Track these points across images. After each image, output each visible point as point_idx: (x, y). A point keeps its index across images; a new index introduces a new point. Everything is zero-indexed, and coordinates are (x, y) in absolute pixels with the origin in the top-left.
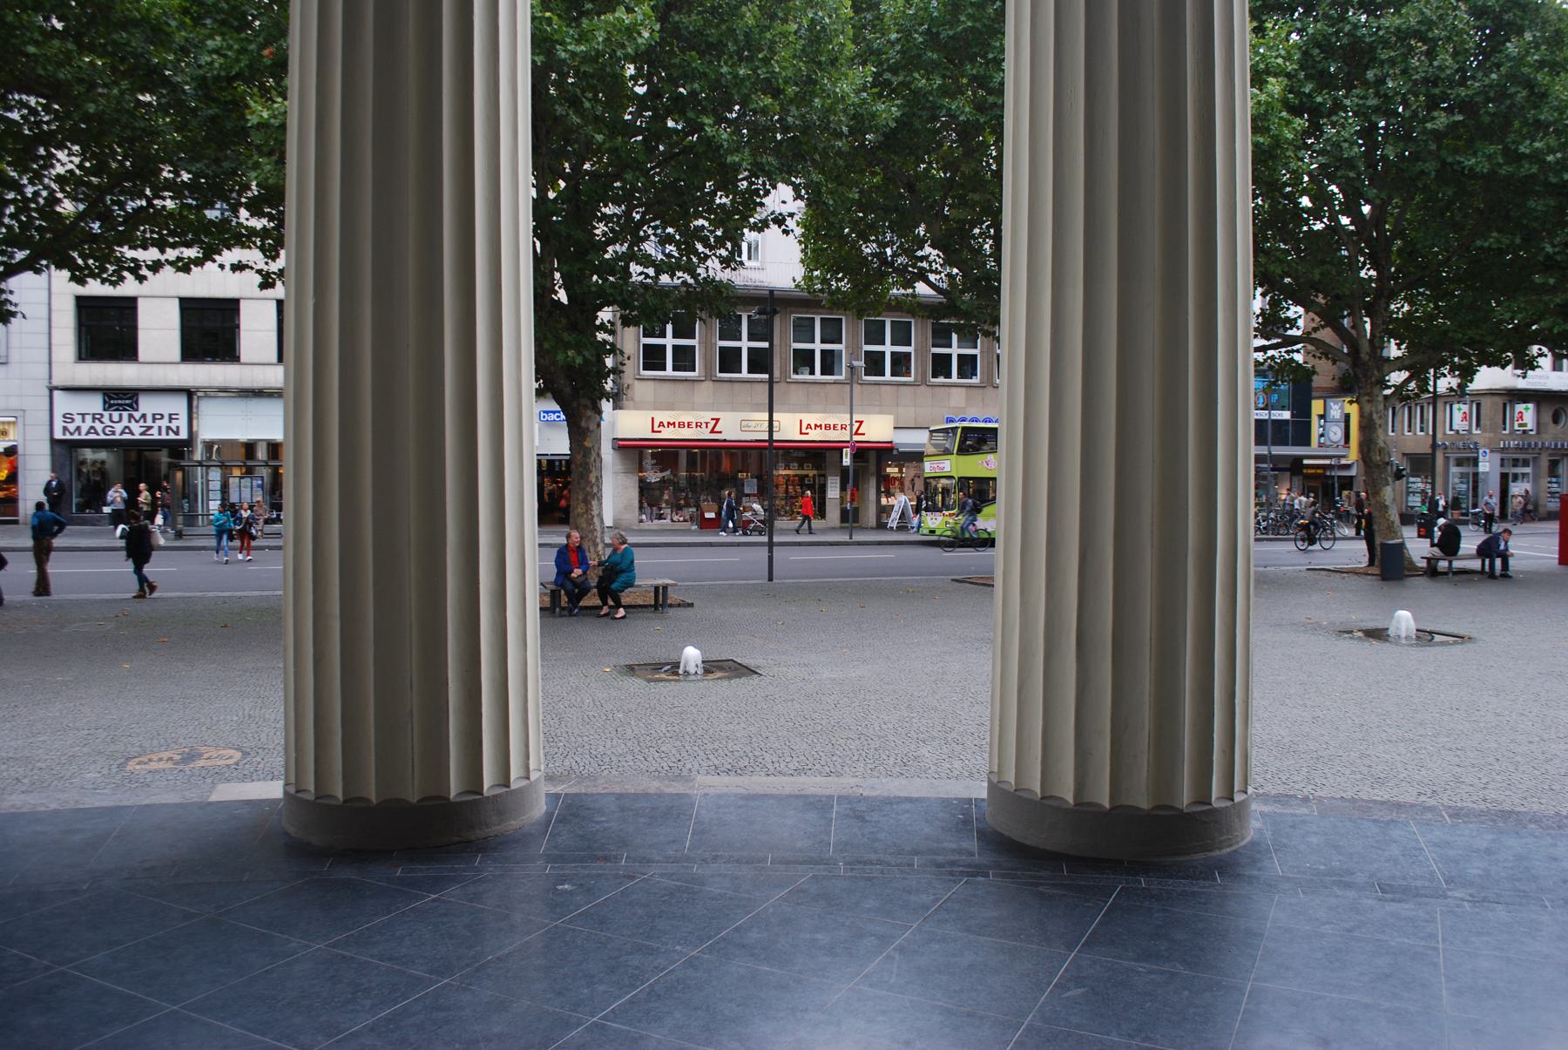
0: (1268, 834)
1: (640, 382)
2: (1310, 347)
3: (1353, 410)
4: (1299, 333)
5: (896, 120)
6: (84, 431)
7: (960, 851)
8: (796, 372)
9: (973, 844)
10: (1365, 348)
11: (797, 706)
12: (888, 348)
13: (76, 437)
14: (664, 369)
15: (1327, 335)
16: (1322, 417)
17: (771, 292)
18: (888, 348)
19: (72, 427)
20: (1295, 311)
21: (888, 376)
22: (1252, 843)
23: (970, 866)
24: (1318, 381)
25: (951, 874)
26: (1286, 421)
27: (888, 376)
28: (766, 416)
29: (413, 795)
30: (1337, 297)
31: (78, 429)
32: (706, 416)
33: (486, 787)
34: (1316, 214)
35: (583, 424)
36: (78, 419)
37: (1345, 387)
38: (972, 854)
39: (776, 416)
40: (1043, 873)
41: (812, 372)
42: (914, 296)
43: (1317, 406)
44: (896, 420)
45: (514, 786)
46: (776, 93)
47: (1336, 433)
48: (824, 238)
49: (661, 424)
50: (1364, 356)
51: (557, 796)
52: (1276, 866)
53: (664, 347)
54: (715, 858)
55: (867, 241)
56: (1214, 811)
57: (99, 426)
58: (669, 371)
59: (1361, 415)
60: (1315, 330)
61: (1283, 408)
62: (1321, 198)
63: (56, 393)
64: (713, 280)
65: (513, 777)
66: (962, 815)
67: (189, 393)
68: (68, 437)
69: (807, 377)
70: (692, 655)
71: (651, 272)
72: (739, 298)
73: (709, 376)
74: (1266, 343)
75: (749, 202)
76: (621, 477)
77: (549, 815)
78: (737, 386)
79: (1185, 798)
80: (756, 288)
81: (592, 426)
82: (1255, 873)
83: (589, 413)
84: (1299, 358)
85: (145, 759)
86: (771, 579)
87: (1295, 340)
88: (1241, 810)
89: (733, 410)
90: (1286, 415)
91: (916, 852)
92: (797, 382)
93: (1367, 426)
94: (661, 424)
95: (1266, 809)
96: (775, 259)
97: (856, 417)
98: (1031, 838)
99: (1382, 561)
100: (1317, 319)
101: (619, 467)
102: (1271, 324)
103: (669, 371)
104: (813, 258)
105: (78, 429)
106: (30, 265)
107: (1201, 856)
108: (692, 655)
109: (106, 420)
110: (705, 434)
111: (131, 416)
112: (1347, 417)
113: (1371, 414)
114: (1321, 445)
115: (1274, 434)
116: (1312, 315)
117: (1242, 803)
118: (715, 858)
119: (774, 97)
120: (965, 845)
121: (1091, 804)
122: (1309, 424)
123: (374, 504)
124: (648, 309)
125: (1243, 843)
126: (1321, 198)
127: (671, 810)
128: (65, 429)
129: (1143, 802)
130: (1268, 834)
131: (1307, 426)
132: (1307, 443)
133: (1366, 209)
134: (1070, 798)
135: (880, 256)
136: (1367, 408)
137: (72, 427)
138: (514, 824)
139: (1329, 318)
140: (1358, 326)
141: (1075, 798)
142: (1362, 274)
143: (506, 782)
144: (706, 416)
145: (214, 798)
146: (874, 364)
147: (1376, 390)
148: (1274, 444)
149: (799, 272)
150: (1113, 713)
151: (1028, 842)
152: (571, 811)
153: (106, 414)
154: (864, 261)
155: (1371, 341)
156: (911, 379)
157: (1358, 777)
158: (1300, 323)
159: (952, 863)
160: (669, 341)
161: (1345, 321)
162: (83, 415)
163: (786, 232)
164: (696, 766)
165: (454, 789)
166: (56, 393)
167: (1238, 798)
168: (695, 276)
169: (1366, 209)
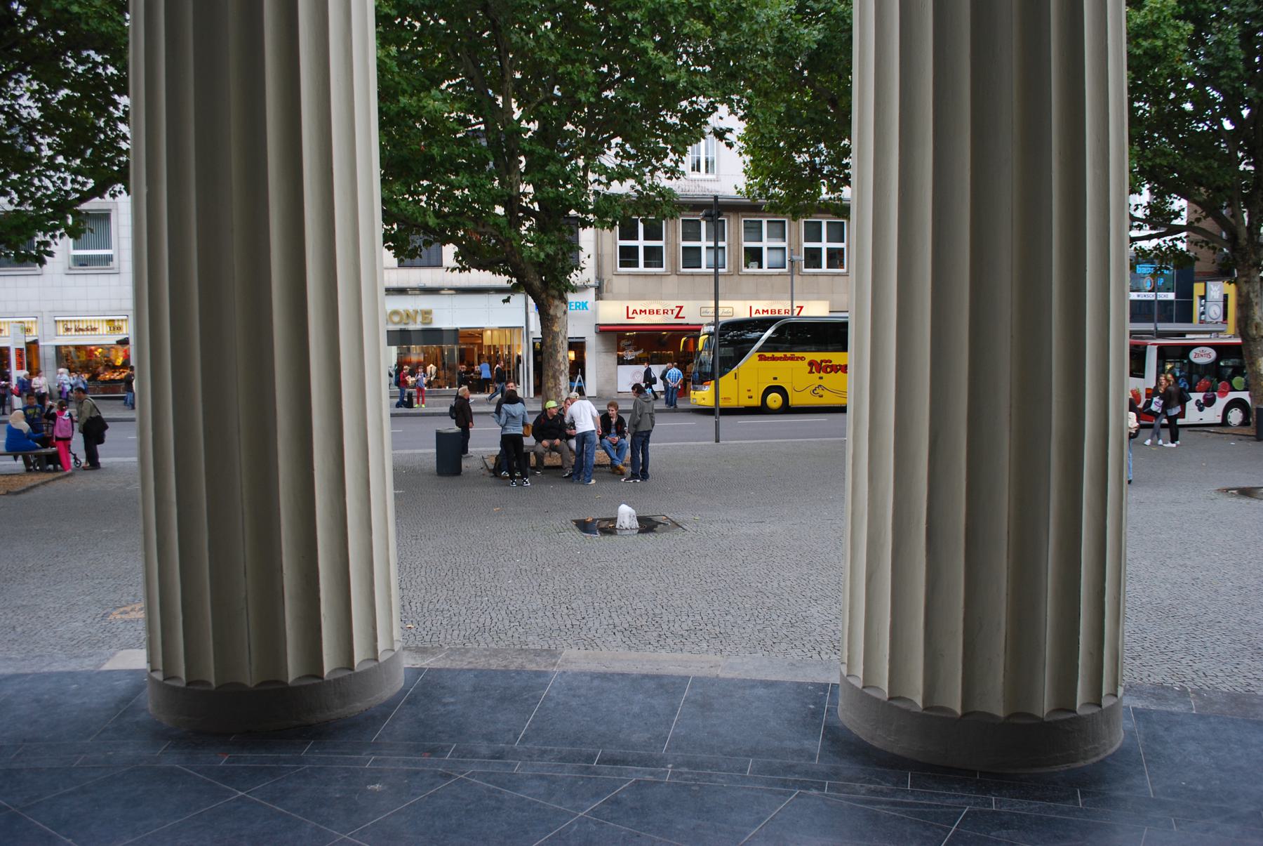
0: (1140, 739)
1: (620, 278)
2: (1195, 237)
3: (1231, 290)
4: (1184, 223)
5: (819, 43)
7: (800, 753)
8: (747, 266)
9: (816, 745)
10: (1243, 234)
11: (708, 561)
12: (824, 245)
15: (1209, 224)
16: (1203, 297)
17: (716, 197)
18: (824, 245)
20: (1179, 204)
21: (824, 268)
22: (1123, 751)
23: (806, 773)
24: (1198, 267)
25: (784, 784)
26: (1171, 302)
27: (824, 268)
28: (712, 303)
29: (249, 677)
30: (1219, 189)
32: (672, 305)
33: (326, 671)
34: (1198, 115)
35: (552, 312)
37: (1223, 273)
38: (812, 757)
39: (721, 303)
40: (885, 787)
41: (760, 266)
42: (840, 199)
43: (1198, 288)
44: (831, 305)
45: (381, 659)
46: (708, 20)
47: (1215, 311)
48: (764, 152)
49: (635, 311)
50: (1243, 241)
51: (420, 671)
52: (1148, 784)
53: (637, 248)
54: (543, 753)
55: (800, 152)
56: (1080, 718)
58: (641, 268)
59: (1239, 294)
60: (1198, 220)
61: (1168, 290)
62: (1202, 102)
64: (658, 186)
65: (357, 660)
66: (813, 702)
69: (755, 270)
70: (626, 514)
71: (603, 179)
73: (676, 272)
74: (1153, 232)
75: (696, 119)
76: (604, 357)
77: (403, 692)
78: (697, 278)
79: (1044, 705)
80: (704, 196)
81: (560, 314)
82: (1121, 793)
83: (557, 302)
84: (1182, 246)
85: (128, 609)
86: (717, 441)
87: (1180, 229)
88: (1108, 716)
89: (695, 299)
90: (1171, 296)
91: (753, 752)
92: (747, 275)
93: (1245, 305)
94: (635, 311)
95: (1139, 704)
96: (719, 166)
97: (796, 303)
98: (880, 740)
99: (1258, 422)
100: (1200, 210)
101: (601, 348)
102: (1159, 218)
103: (641, 268)
104: (756, 169)
107: (1064, 767)
108: (626, 514)
110: (671, 319)
112: (1226, 297)
113: (1248, 293)
114: (1201, 322)
115: (1159, 314)
116: (1195, 207)
117: (1111, 708)
118: (543, 753)
119: (706, 24)
120: (808, 744)
121: (942, 709)
122: (1192, 303)
124: (618, 215)
125: (1110, 751)
126: (1202, 102)
127: (511, 690)
129: (997, 707)
130: (1140, 739)
131: (1190, 305)
132: (1189, 319)
133: (1245, 113)
134: (919, 701)
135: (811, 164)
136: (1245, 289)
138: (359, 706)
139: (1209, 208)
140: (1236, 215)
141: (924, 702)
142: (1242, 167)
143: (318, 673)
144: (672, 305)
145: (108, 666)
146: (813, 258)
147: (1253, 272)
148: (1160, 321)
149: (742, 181)
150: (965, 613)
151: (876, 744)
152: (427, 688)
154: (798, 168)
155: (1248, 228)
156: (844, 270)
157: (1238, 646)
158: (1184, 214)
159: (789, 769)
160: (641, 243)
161: (1224, 212)
163: (730, 145)
164: (597, 624)
165: (293, 671)
167: (1107, 702)
168: (641, 183)
169: (1245, 113)
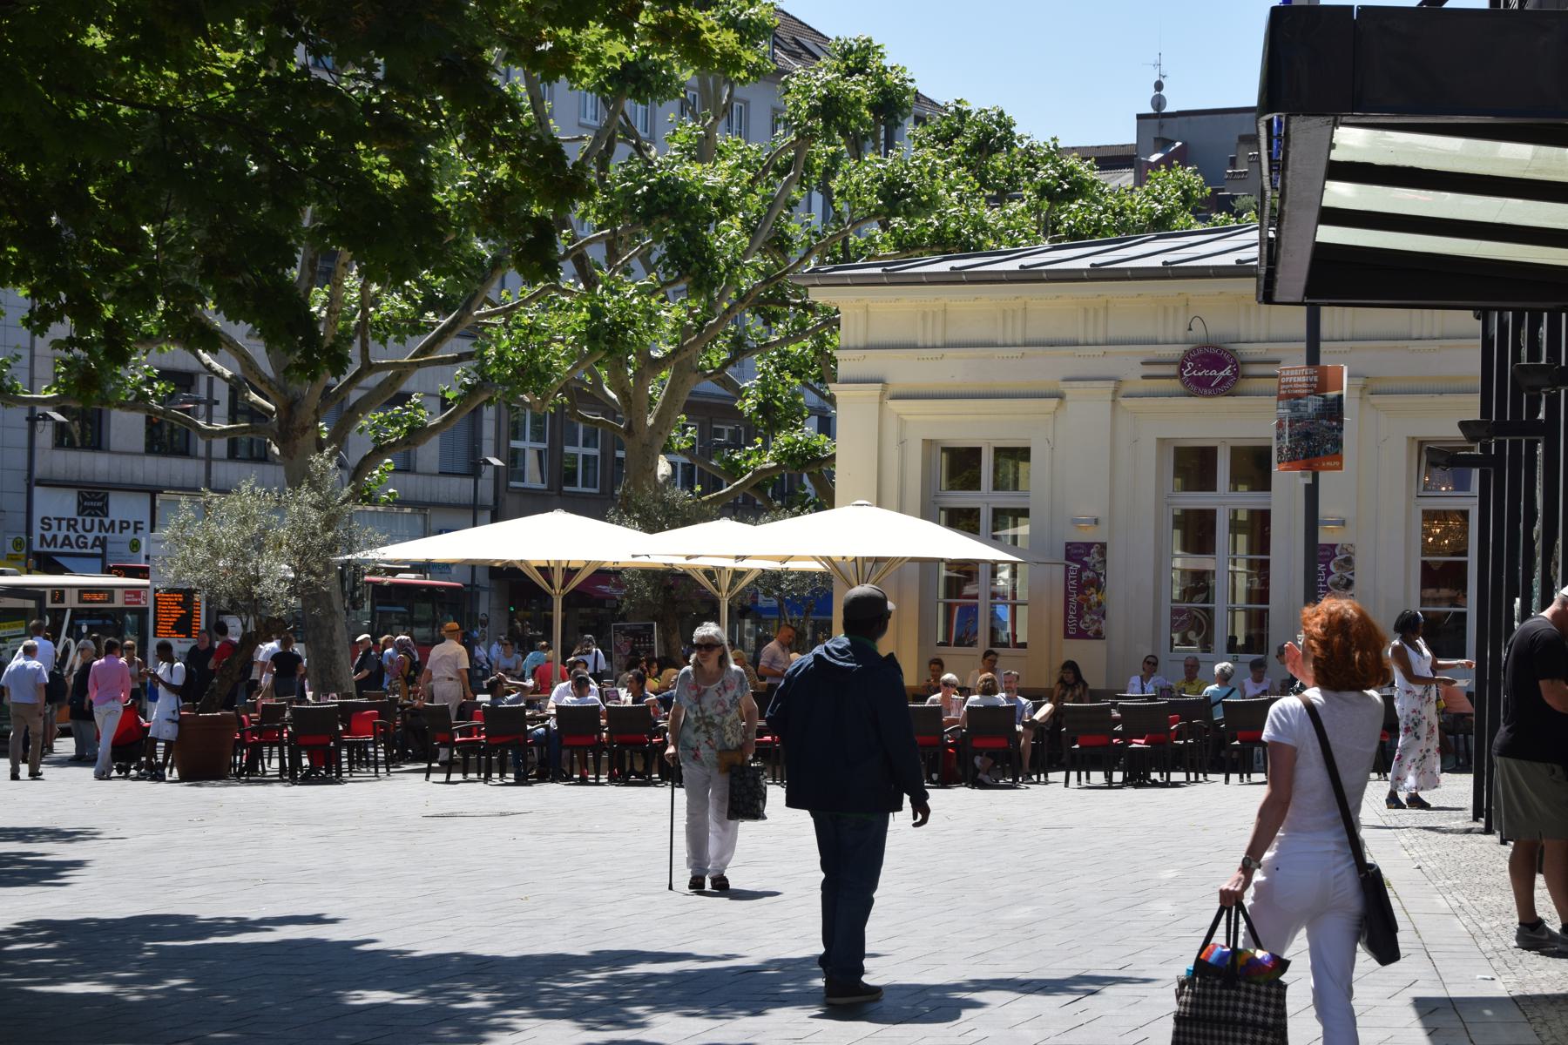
6: (60, 540)
13: (52, 549)
14: (575, 485)
19: (49, 536)
31: (55, 537)
36: (55, 523)
57: (73, 535)
63: (37, 490)
67: (153, 491)
68: (45, 549)
72: (602, 403)
105: (55, 537)
106: (172, 341)
109: (79, 527)
111: (101, 523)
123: (1464, 636)
128: (43, 537)
137: (49, 536)
153: (80, 519)
156: (596, 491)
162: (60, 520)
166: (37, 490)
